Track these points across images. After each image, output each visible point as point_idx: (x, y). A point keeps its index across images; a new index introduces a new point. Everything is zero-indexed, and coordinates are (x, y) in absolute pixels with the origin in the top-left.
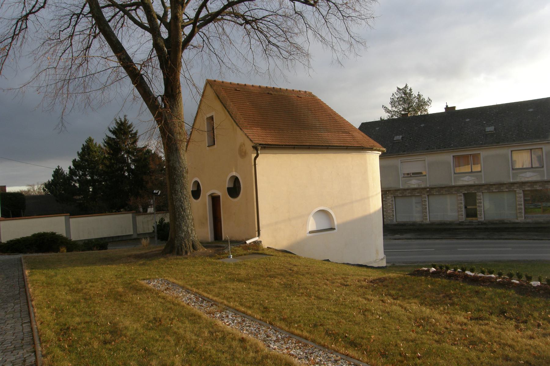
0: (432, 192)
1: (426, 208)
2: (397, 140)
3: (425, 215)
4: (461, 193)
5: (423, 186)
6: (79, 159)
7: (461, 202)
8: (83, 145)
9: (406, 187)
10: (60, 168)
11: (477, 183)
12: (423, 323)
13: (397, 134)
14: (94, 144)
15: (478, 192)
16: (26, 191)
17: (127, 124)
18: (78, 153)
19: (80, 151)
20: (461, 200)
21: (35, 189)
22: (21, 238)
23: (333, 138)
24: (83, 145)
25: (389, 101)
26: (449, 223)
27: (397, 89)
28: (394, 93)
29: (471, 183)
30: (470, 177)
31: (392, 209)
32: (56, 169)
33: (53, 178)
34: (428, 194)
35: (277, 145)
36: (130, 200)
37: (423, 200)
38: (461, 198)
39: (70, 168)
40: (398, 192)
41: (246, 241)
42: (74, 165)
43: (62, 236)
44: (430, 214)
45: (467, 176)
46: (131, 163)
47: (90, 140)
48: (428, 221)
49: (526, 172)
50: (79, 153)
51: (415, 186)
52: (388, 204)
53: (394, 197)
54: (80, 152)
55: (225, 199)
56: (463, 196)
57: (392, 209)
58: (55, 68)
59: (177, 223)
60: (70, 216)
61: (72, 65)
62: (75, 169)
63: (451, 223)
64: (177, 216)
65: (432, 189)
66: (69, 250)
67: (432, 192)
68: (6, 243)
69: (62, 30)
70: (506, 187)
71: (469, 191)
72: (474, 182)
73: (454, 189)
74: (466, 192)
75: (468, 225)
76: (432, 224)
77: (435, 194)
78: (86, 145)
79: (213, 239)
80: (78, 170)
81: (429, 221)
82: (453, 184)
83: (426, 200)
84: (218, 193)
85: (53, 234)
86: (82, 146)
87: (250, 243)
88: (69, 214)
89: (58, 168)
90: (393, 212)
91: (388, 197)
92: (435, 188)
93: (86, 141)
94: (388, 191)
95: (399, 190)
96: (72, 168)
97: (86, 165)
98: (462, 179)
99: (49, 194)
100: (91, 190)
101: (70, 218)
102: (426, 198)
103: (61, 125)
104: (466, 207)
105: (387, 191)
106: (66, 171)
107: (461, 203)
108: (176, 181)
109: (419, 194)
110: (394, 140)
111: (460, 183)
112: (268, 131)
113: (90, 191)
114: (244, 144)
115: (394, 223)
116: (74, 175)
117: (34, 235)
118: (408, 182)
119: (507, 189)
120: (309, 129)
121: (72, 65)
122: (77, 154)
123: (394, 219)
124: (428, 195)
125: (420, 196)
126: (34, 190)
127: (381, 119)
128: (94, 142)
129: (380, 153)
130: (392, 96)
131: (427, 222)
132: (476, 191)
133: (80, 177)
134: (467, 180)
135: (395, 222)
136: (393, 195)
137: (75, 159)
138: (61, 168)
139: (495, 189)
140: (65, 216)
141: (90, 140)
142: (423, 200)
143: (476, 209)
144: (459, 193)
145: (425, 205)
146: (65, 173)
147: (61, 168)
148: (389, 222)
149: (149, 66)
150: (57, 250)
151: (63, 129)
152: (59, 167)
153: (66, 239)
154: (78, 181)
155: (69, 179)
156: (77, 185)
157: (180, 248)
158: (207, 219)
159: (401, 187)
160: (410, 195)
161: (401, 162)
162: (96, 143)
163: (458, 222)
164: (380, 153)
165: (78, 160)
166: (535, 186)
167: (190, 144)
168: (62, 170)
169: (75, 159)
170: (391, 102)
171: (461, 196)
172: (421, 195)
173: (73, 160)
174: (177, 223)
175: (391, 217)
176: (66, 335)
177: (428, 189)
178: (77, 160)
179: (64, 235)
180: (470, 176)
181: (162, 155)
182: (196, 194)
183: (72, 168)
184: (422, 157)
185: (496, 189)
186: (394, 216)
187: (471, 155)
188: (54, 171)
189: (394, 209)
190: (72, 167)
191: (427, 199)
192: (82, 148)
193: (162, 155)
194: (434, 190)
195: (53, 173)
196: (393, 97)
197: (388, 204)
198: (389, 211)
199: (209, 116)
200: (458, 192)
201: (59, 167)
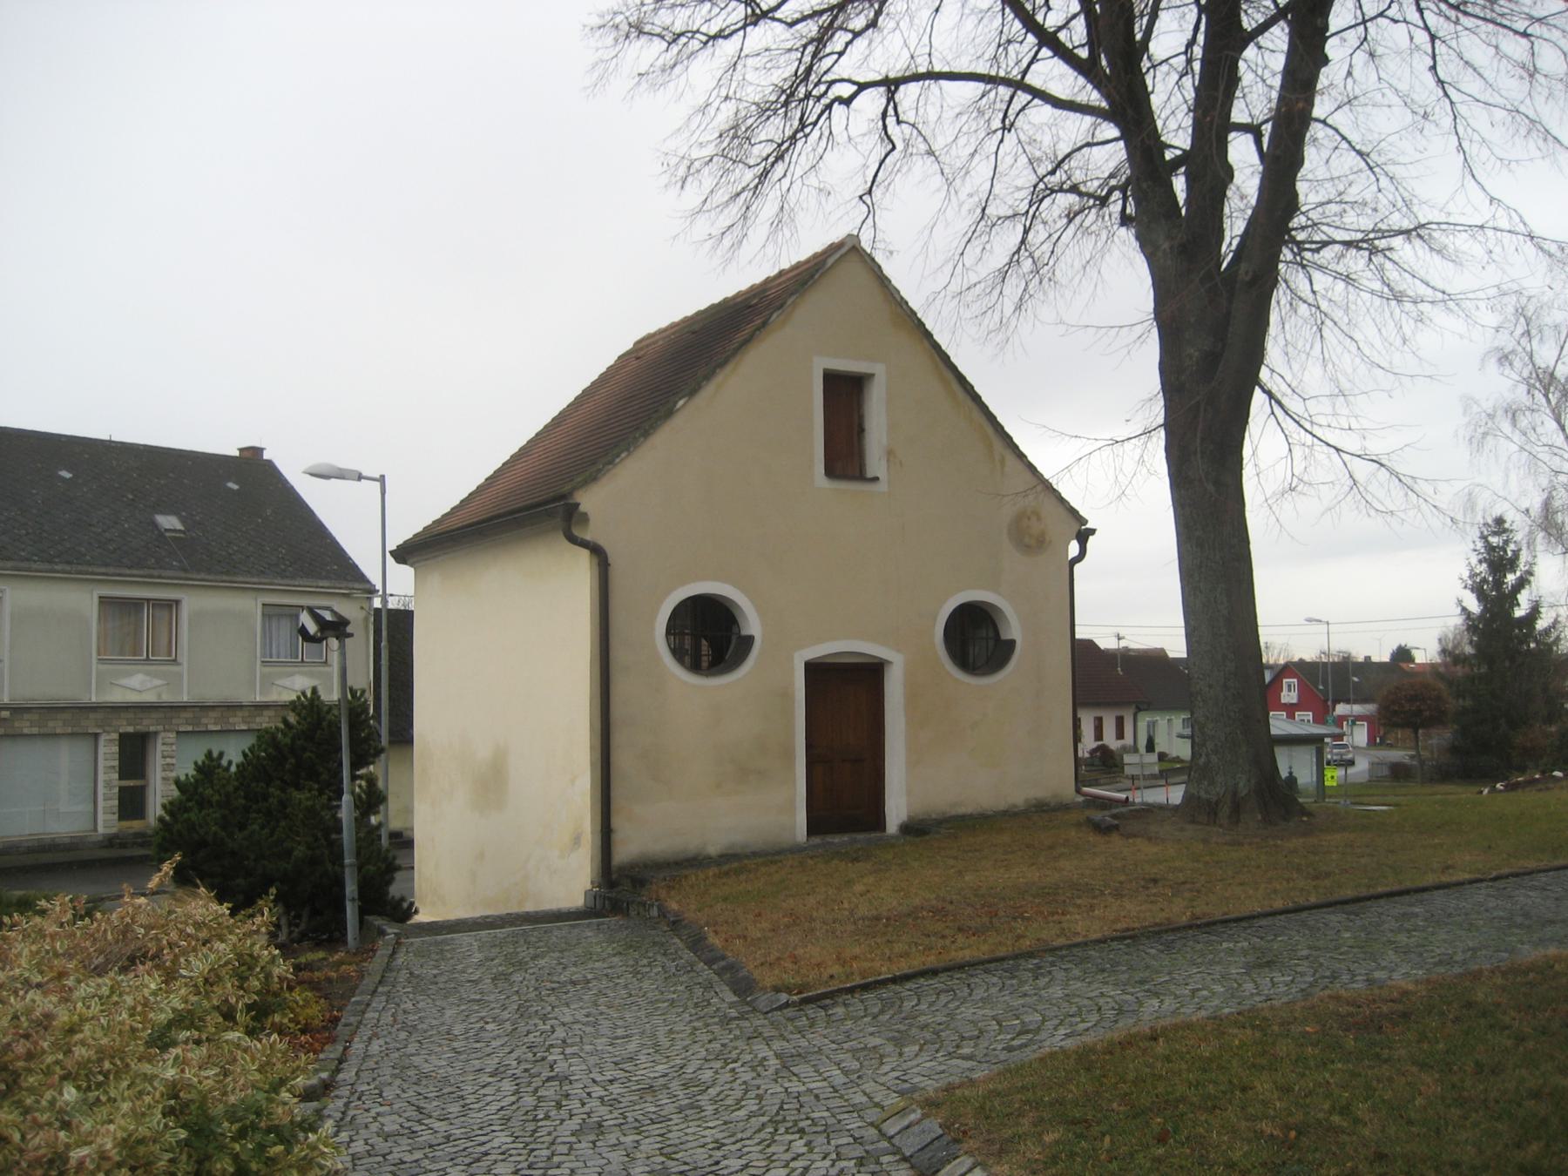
11: (167, 697)
12: (1211, 1004)
13: (63, 479)
14: (1519, 613)
15: (165, 731)
26: (67, 841)
29: (149, 697)
30: (148, 678)
41: (1125, 756)
45: (139, 672)
49: (292, 674)
67: (17, 724)
68: (1103, 651)
70: (243, 717)
71: (138, 727)
72: (159, 696)
73: (92, 716)
77: (26, 731)
82: (94, 700)
92: (28, 710)
98: (124, 682)
106: (1420, 658)
111: (116, 696)
119: (129, 725)
132: (160, 728)
134: (138, 686)
143: (121, 778)
144: (108, 732)
166: (231, 720)
167: (1340, 110)
176: (1196, 1089)
180: (148, 673)
181: (1183, 169)
185: (215, 724)
187: (148, 600)
193: (1183, 169)
194: (26, 716)
200: (107, 728)
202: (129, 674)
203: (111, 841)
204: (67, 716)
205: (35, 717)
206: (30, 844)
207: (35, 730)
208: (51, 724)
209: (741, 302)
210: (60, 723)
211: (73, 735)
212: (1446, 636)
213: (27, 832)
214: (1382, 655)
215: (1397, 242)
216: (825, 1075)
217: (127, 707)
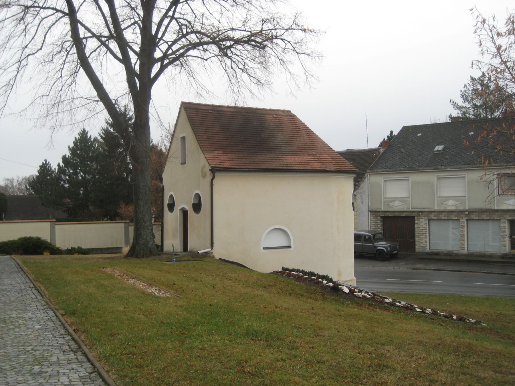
0: (471, 216)
1: (464, 235)
2: (437, 151)
3: (462, 243)
4: (505, 219)
5: (461, 208)
6: (70, 155)
7: (504, 230)
8: (76, 138)
9: (442, 208)
10: (47, 162)
14: (88, 137)
16: (2, 187)
17: (128, 115)
18: (69, 147)
19: (72, 145)
20: (505, 227)
21: (14, 185)
22: (8, 241)
23: (294, 161)
24: (76, 138)
25: (459, 95)
26: (489, 254)
27: (470, 79)
28: (466, 84)
31: (425, 235)
32: (43, 164)
33: (37, 174)
34: (467, 218)
35: (233, 168)
36: (121, 208)
37: (461, 225)
38: (504, 225)
39: (59, 165)
40: (433, 214)
42: (63, 162)
43: (47, 242)
44: (469, 242)
46: (129, 163)
47: (84, 134)
48: (465, 251)
50: (71, 147)
51: (453, 208)
52: (421, 228)
53: (429, 220)
54: (71, 147)
55: (191, 213)
56: (507, 223)
57: (425, 235)
58: (48, 95)
59: (139, 232)
60: (56, 222)
61: (62, 87)
62: (65, 166)
63: (491, 256)
64: (139, 226)
65: (471, 212)
66: (52, 253)
69: (55, 54)
73: (496, 214)
74: (510, 218)
75: (510, 258)
76: (470, 255)
77: (474, 218)
78: (79, 138)
79: (182, 250)
80: (68, 168)
81: (429, 249)
82: (496, 208)
83: (464, 226)
84: (187, 208)
85: (38, 239)
86: (74, 140)
87: (202, 253)
88: (55, 220)
89: (44, 162)
90: (426, 238)
91: (421, 220)
92: (475, 211)
93: (79, 134)
94: (422, 212)
95: (434, 211)
96: (61, 166)
97: (77, 163)
98: (507, 202)
99: (34, 194)
100: (81, 192)
101: (55, 224)
102: (464, 223)
103: (50, 143)
104: (511, 237)
105: (420, 212)
106: (55, 167)
107: (505, 231)
108: (140, 197)
109: (456, 218)
110: (435, 150)
111: (504, 207)
112: (229, 155)
113: (80, 194)
114: (205, 166)
115: (426, 251)
116: (62, 174)
117: (20, 239)
118: (444, 203)
120: (272, 152)
121: (62, 87)
122: (68, 149)
123: (427, 246)
124: (467, 220)
125: (458, 220)
126: (13, 186)
127: (450, 117)
128: (89, 135)
129: (355, 176)
130: (464, 88)
131: (464, 253)
133: (70, 176)
135: (427, 250)
136: (426, 218)
137: (65, 155)
138: (49, 162)
139: (454, 216)
140: (51, 222)
141: (84, 134)
142: (461, 225)
144: (502, 219)
145: (463, 231)
146: (53, 169)
147: (49, 162)
148: (421, 249)
149: (172, 18)
150: (41, 253)
151: (52, 147)
152: (46, 161)
153: (50, 244)
154: (69, 182)
155: (58, 179)
156: (66, 186)
157: (139, 252)
158: (178, 231)
159: (436, 209)
160: (446, 218)
161: (438, 178)
162: (91, 136)
163: (500, 255)
164: (355, 176)
165: (69, 156)
168: (50, 165)
169: (65, 155)
170: (463, 96)
171: (504, 222)
172: (458, 220)
173: (63, 156)
174: (139, 232)
175: (424, 243)
177: (467, 213)
178: (67, 157)
179: (49, 240)
182: (171, 207)
183: (61, 166)
184: (459, 174)
186: (426, 242)
188: (40, 166)
189: (428, 235)
190: (62, 164)
191: (465, 224)
192: (74, 142)
195: (39, 168)
196: (466, 89)
197: (421, 228)
198: (421, 237)
199: (182, 135)
201: (46, 161)
202: (509, 200)
203: (504, 256)
204: (488, 213)
205: (477, 214)
206: (476, 254)
207: (477, 218)
208: (482, 216)
209: (223, 111)
210: (486, 216)
211: (437, 220)
212: (157, 147)
213: (479, 250)
214: (34, 172)
215: (73, 79)
216: (23, 319)
217: (509, 211)
